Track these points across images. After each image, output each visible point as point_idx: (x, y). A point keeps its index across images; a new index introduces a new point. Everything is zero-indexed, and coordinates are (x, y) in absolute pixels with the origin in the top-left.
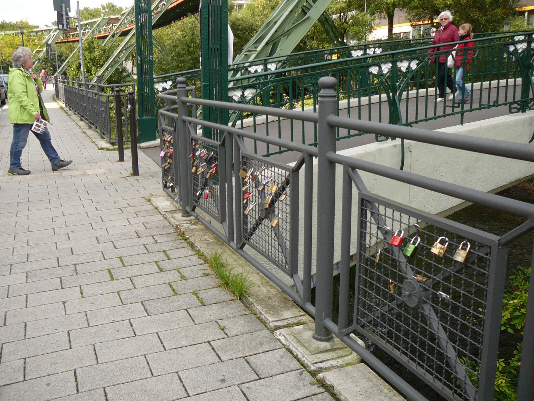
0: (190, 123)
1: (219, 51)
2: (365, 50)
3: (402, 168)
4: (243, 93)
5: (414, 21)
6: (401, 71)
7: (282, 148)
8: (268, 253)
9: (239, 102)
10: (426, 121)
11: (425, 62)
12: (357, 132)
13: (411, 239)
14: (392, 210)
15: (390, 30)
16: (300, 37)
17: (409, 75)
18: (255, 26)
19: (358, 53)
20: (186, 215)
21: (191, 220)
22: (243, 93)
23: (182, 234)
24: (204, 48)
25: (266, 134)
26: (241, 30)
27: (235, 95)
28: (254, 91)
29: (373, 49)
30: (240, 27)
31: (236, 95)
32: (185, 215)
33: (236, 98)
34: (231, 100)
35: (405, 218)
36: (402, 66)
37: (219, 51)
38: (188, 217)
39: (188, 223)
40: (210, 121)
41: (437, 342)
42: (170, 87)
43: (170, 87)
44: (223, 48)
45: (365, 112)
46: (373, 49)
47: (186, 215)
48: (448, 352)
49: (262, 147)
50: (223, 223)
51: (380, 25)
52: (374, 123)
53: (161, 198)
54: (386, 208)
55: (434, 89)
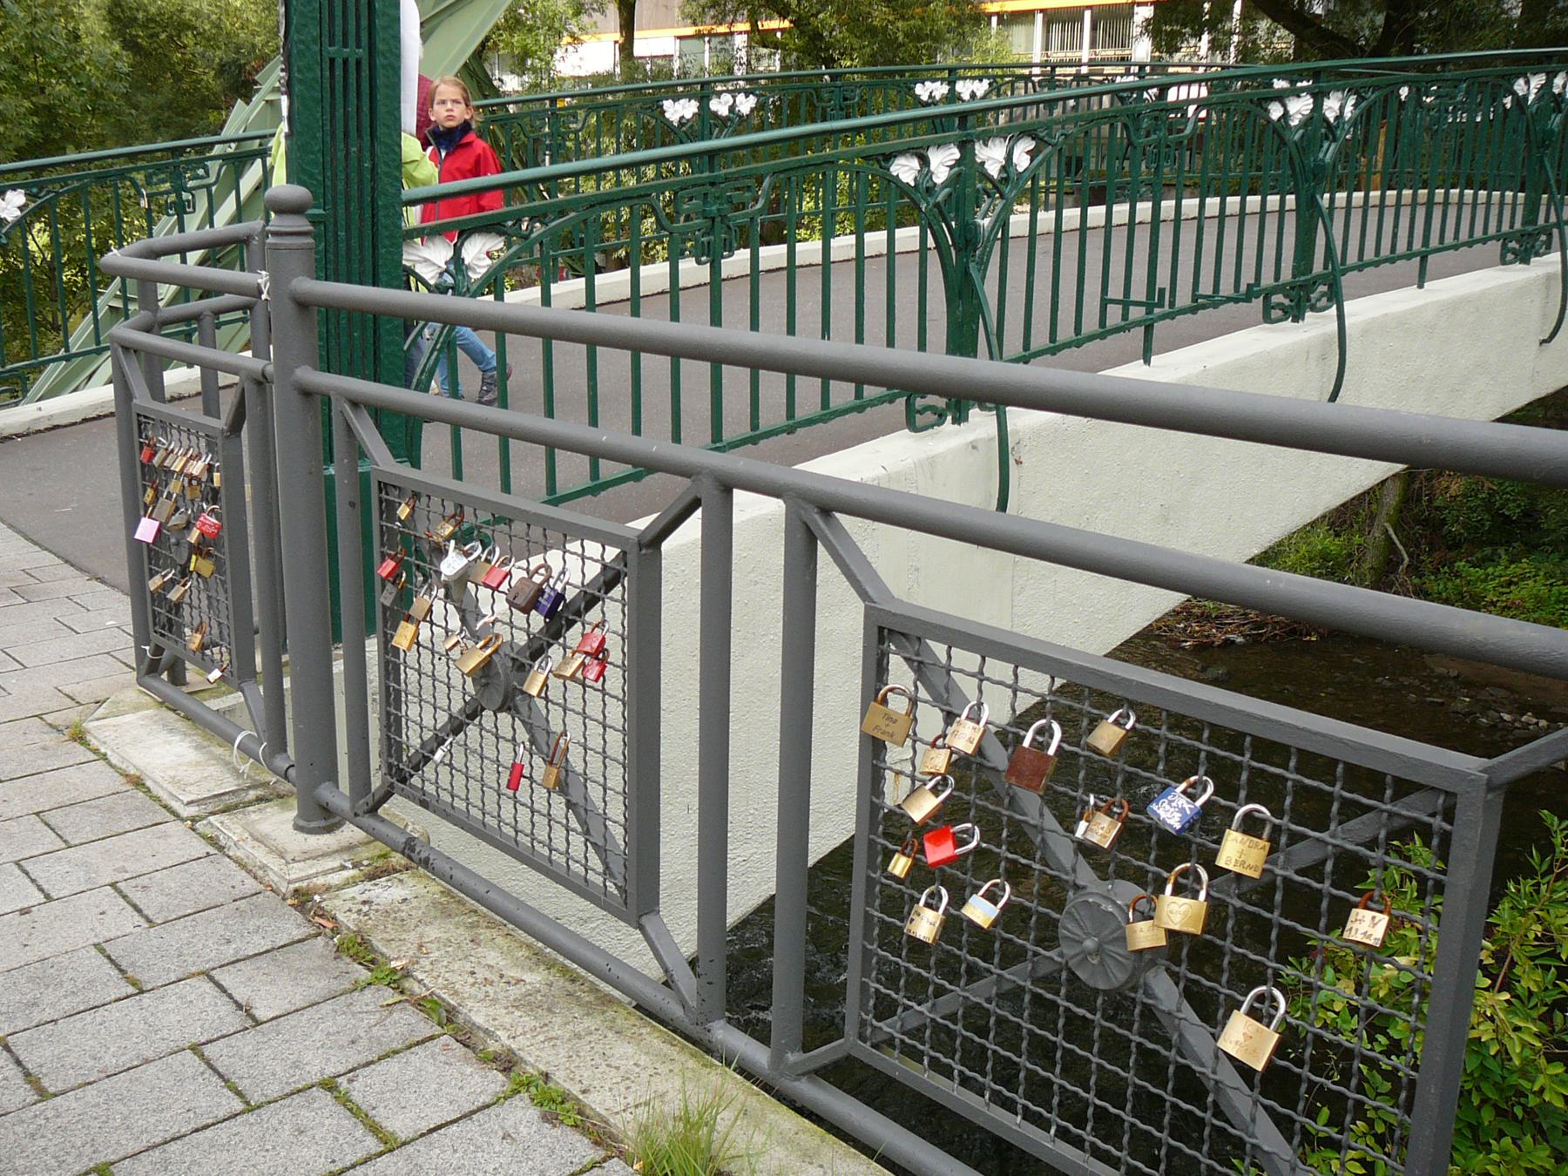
0: (355, 404)
1: (365, 73)
2: (704, 100)
3: (1002, 505)
4: (457, 250)
5: (703, 23)
6: (988, 178)
7: (603, 464)
8: (480, 817)
9: (441, 289)
10: (1078, 347)
11: (1056, 145)
12: (882, 391)
13: (1022, 733)
14: (979, 657)
15: (626, 48)
16: (462, 50)
17: (1011, 191)
18: (192, 13)
19: (684, 108)
20: (322, 823)
21: (350, 848)
22: (457, 250)
23: (359, 949)
24: (301, 54)
25: (629, 427)
26: (144, 26)
27: (426, 260)
28: (496, 243)
29: (727, 98)
30: (140, 15)
31: (430, 258)
32: (313, 825)
33: (430, 275)
34: (405, 277)
35: (593, 549)
36: (989, 158)
37: (365, 73)
38: (329, 830)
39: (343, 868)
40: (376, 379)
41: (1214, 1101)
42: (18, 213)
43: (18, 213)
44: (380, 61)
45: (735, 303)
46: (727, 98)
47: (322, 823)
48: (1257, 1132)
49: (528, 464)
50: (644, 920)
51: (595, 29)
52: (905, 357)
53: (129, 718)
54: (1017, 667)
55: (916, 230)
